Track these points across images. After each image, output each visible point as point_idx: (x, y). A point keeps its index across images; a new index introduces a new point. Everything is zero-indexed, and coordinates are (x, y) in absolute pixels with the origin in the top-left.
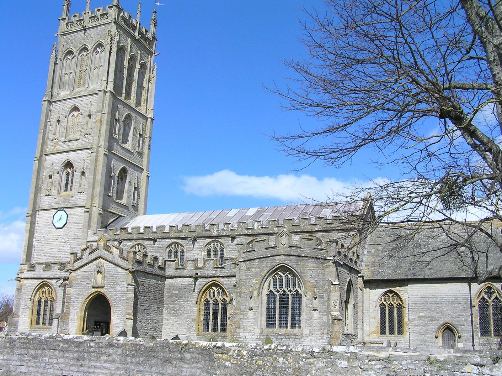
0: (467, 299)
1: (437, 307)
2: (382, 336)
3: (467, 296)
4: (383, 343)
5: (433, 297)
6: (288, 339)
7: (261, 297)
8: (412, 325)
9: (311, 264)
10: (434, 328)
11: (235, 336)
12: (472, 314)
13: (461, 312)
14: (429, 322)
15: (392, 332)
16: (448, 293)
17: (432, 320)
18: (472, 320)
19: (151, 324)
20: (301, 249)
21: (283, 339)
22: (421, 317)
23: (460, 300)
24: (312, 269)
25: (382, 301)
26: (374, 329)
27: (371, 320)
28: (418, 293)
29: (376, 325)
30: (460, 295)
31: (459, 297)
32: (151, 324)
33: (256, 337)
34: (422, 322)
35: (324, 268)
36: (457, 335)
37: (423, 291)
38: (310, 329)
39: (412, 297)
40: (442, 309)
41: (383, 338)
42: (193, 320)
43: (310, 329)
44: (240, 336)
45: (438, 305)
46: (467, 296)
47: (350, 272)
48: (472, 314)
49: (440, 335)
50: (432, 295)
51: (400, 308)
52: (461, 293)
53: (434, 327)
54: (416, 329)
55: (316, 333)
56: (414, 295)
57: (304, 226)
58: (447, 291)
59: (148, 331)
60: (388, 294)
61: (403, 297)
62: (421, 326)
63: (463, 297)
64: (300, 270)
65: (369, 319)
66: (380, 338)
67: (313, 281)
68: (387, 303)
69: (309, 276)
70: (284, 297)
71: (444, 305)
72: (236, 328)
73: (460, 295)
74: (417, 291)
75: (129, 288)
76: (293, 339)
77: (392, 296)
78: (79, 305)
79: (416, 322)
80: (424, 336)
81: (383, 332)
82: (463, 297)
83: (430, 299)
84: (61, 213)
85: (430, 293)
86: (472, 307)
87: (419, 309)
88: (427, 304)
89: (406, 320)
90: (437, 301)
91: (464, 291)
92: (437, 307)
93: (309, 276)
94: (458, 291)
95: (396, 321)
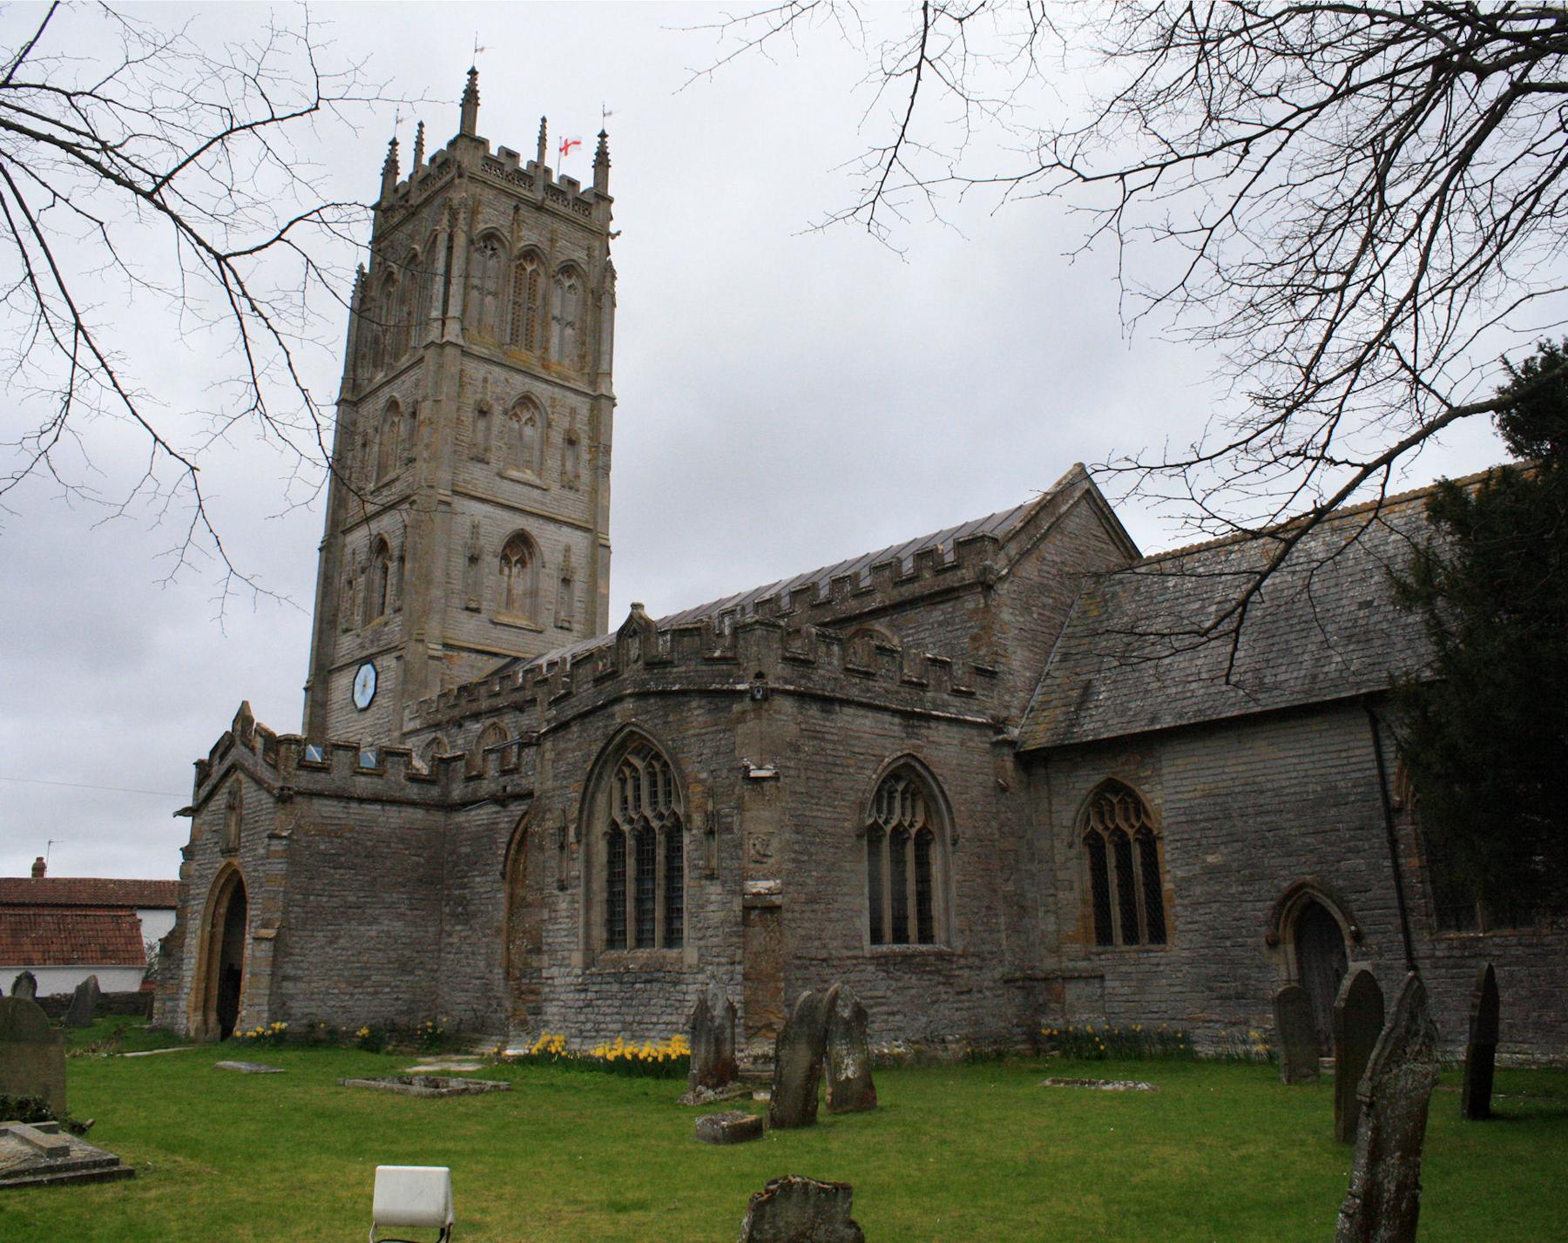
0: (1370, 784)
1: (1264, 827)
2: (1101, 949)
3: (1368, 772)
4: (1102, 978)
5: (1248, 788)
6: (649, 986)
7: (588, 845)
8: (1186, 902)
9: (697, 714)
10: (1263, 909)
11: (524, 981)
12: (1394, 842)
13: (1353, 838)
14: (1240, 889)
15: (1131, 937)
16: (1299, 767)
17: (1251, 879)
18: (1396, 866)
19: (379, 950)
20: (675, 670)
21: (637, 986)
22: (1212, 872)
23: (1344, 791)
24: (704, 731)
25: (1092, 823)
26: (1070, 928)
27: (1061, 895)
28: (1196, 780)
29: (1078, 913)
30: (1341, 769)
31: (1339, 777)
32: (379, 950)
33: (575, 981)
34: (1217, 888)
35: (731, 726)
36: (1347, 929)
37: (1211, 771)
38: (700, 948)
39: (1180, 796)
40: (1281, 833)
41: (1103, 957)
42: (498, 931)
43: (700, 948)
44: (540, 977)
45: (1268, 819)
46: (1368, 772)
47: (521, 710)
48: (1394, 842)
49: (1288, 934)
50: (1242, 781)
51: (1150, 843)
52: (1345, 762)
53: (1259, 905)
54: (1197, 918)
55: (716, 960)
56: (1182, 789)
57: (844, 600)
58: (1296, 761)
59: (366, 972)
60: (1108, 795)
61: (1153, 800)
62: (1215, 906)
63: (1353, 775)
64: (673, 740)
65: (1052, 891)
66: (1092, 957)
67: (704, 775)
68: (1133, 827)
69: (695, 759)
70: (645, 836)
71: (1290, 816)
72: (530, 952)
73: (1341, 769)
74: (1190, 774)
75: (272, 848)
76: (659, 985)
77: (1119, 802)
78: (200, 907)
79: (1198, 890)
80: (1228, 943)
81: (1104, 937)
82: (1353, 775)
83: (1240, 798)
84: (367, 670)
85: (1234, 775)
86: (1391, 812)
87: (1204, 842)
88: (1229, 817)
89: (1167, 886)
90: (1262, 802)
91: (1357, 752)
92: (1264, 827)
93: (695, 759)
94: (1334, 755)
95: (1140, 894)
